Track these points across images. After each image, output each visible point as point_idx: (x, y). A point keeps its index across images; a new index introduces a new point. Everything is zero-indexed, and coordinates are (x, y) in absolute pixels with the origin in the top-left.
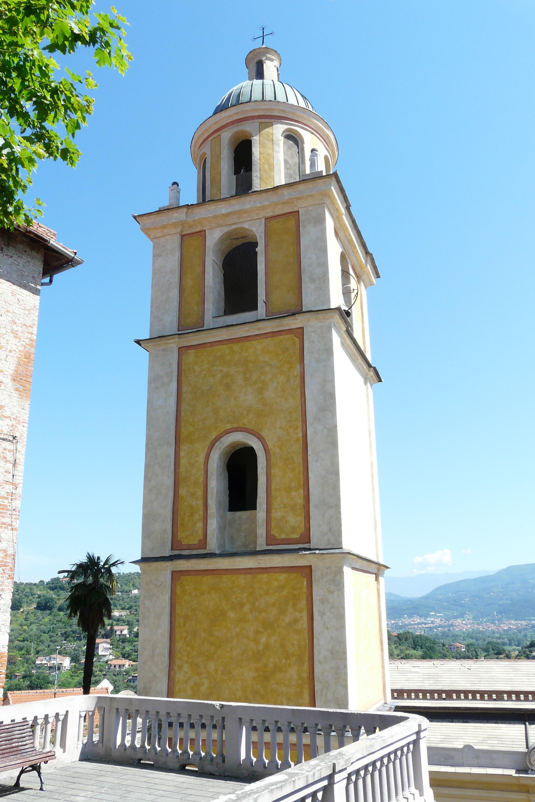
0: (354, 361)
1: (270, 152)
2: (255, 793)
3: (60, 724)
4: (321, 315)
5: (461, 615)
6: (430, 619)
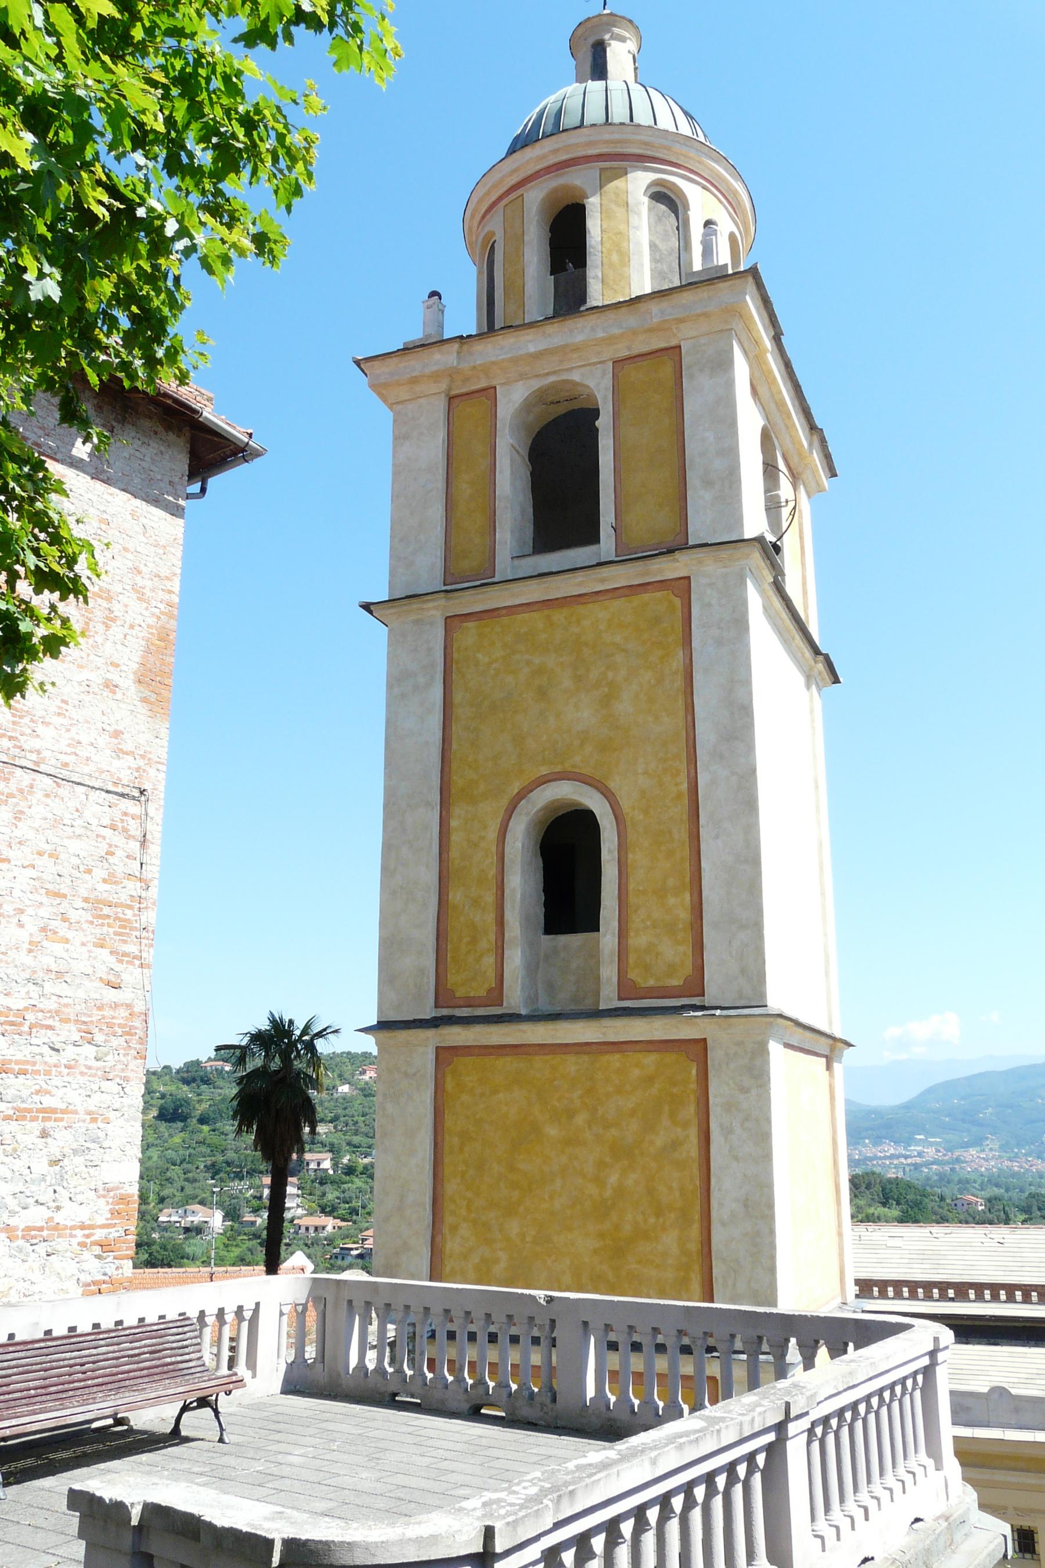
0: (786, 642)
1: (622, 227)
2: (651, 1449)
3: (245, 1325)
4: (724, 553)
5: (978, 1142)
6: (915, 1149)
